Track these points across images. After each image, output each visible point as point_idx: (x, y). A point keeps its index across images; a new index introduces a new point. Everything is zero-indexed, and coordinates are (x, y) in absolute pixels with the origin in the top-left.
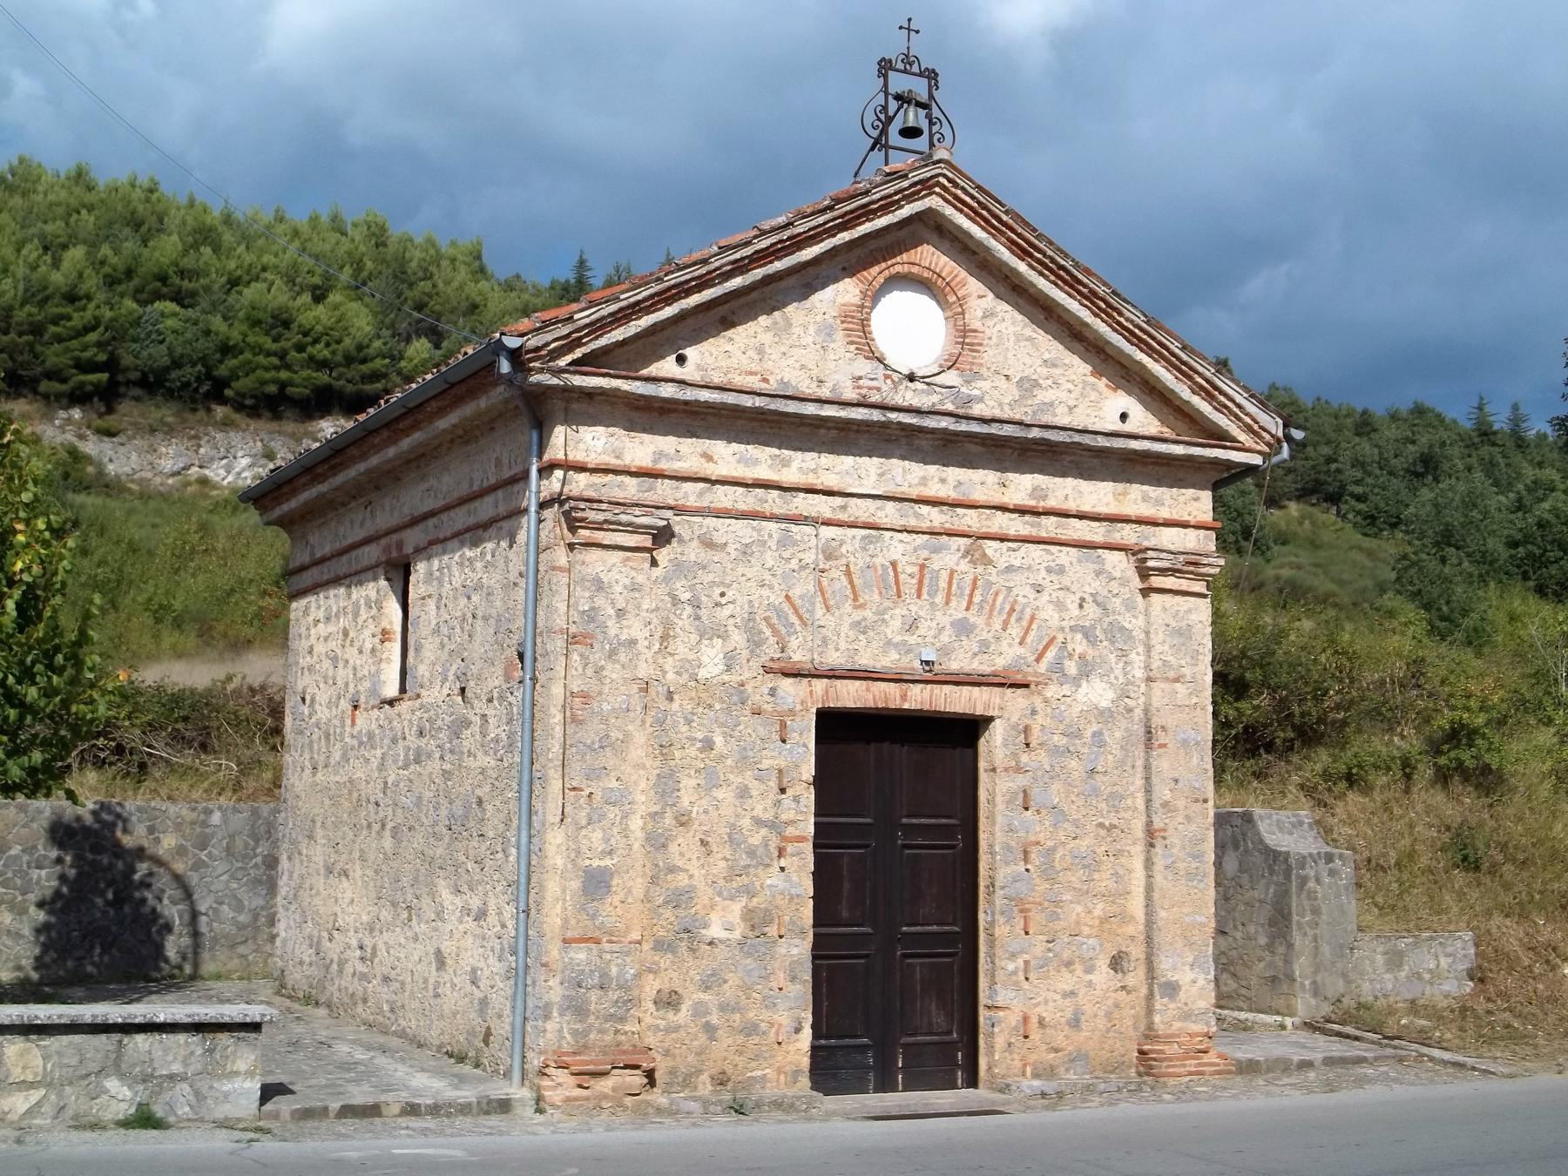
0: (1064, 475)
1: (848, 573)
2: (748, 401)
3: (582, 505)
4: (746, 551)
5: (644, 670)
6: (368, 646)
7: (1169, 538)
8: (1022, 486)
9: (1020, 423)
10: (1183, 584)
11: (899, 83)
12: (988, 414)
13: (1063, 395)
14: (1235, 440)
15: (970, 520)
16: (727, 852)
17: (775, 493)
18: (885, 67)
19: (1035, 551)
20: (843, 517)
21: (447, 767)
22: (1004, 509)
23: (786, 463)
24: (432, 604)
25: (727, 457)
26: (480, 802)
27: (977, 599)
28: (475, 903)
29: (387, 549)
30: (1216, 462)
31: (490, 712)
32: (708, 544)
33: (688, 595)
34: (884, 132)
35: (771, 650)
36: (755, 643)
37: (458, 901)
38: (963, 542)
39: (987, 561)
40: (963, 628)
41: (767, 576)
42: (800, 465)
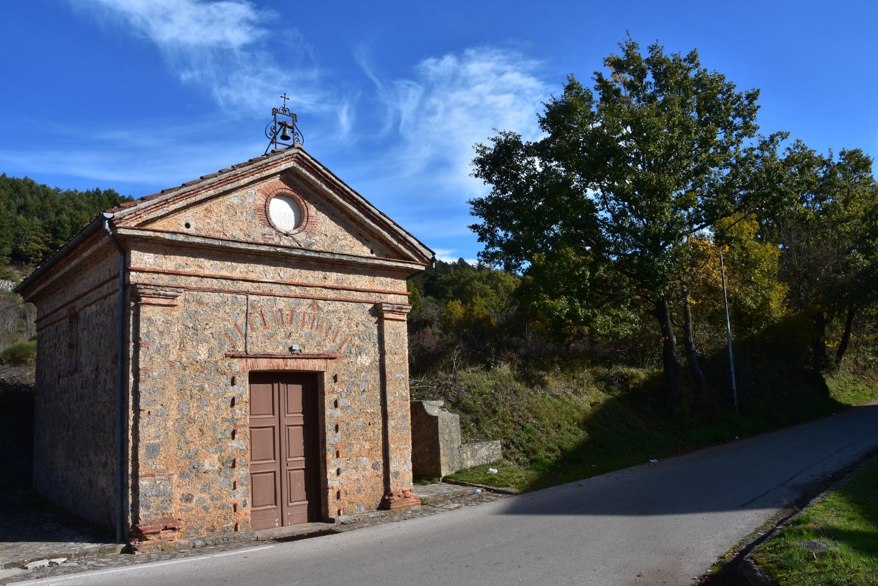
0: (349, 273)
1: (262, 315)
2: (217, 243)
3: (143, 287)
4: (217, 306)
5: (172, 358)
6: (63, 351)
7: (391, 298)
8: (333, 278)
9: (332, 253)
10: (397, 317)
11: (280, 118)
12: (318, 249)
13: (348, 242)
14: (414, 260)
15: (312, 292)
16: (211, 433)
17: (229, 281)
18: (275, 111)
19: (339, 304)
20: (258, 291)
21: (91, 401)
22: (325, 288)
23: (234, 269)
24: (86, 333)
25: (209, 266)
26: (104, 416)
27: (316, 324)
28: (103, 459)
29: (69, 310)
30: (407, 269)
31: (107, 378)
32: (200, 303)
33: (191, 325)
34: (275, 137)
35: (227, 348)
36: (221, 346)
37: (97, 459)
38: (310, 301)
39: (319, 308)
40: (310, 337)
41: (226, 316)
42: (240, 269)
